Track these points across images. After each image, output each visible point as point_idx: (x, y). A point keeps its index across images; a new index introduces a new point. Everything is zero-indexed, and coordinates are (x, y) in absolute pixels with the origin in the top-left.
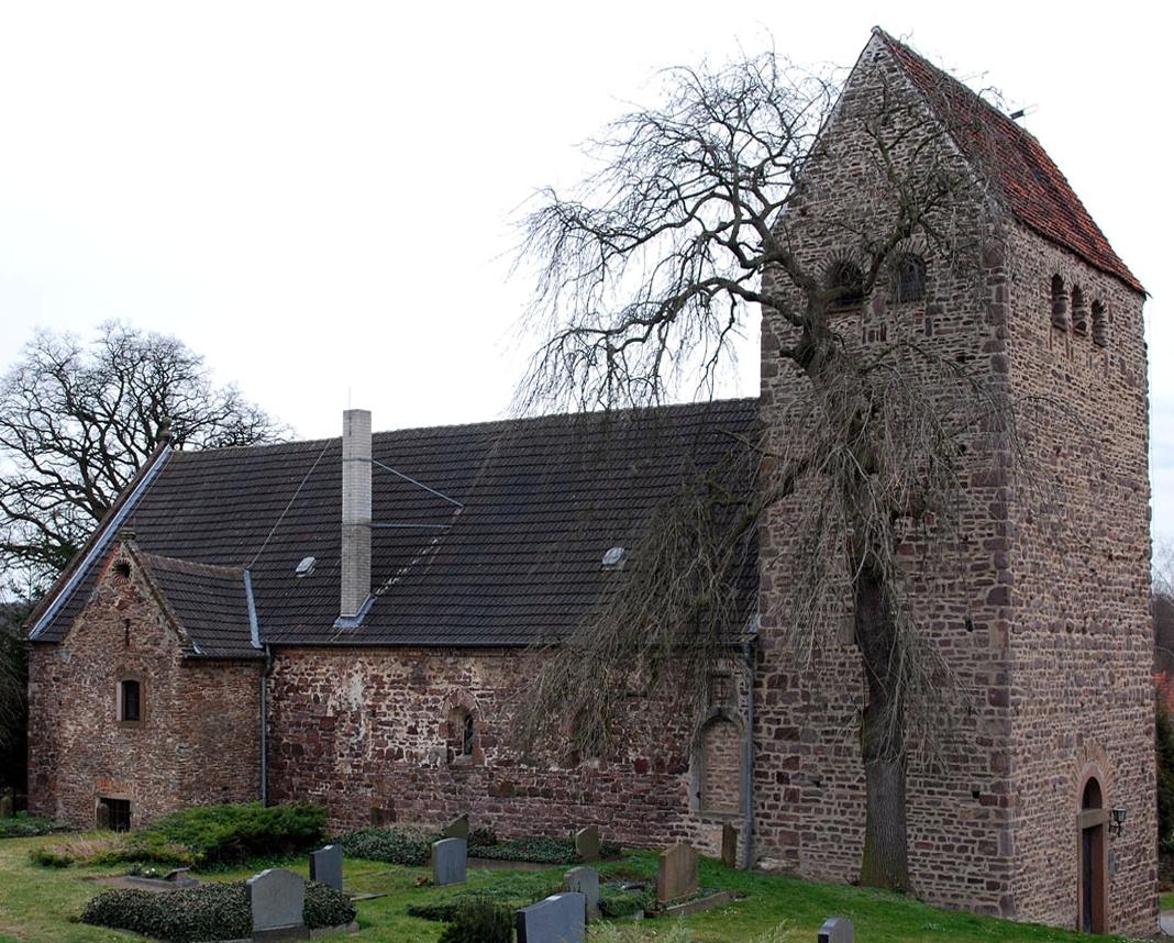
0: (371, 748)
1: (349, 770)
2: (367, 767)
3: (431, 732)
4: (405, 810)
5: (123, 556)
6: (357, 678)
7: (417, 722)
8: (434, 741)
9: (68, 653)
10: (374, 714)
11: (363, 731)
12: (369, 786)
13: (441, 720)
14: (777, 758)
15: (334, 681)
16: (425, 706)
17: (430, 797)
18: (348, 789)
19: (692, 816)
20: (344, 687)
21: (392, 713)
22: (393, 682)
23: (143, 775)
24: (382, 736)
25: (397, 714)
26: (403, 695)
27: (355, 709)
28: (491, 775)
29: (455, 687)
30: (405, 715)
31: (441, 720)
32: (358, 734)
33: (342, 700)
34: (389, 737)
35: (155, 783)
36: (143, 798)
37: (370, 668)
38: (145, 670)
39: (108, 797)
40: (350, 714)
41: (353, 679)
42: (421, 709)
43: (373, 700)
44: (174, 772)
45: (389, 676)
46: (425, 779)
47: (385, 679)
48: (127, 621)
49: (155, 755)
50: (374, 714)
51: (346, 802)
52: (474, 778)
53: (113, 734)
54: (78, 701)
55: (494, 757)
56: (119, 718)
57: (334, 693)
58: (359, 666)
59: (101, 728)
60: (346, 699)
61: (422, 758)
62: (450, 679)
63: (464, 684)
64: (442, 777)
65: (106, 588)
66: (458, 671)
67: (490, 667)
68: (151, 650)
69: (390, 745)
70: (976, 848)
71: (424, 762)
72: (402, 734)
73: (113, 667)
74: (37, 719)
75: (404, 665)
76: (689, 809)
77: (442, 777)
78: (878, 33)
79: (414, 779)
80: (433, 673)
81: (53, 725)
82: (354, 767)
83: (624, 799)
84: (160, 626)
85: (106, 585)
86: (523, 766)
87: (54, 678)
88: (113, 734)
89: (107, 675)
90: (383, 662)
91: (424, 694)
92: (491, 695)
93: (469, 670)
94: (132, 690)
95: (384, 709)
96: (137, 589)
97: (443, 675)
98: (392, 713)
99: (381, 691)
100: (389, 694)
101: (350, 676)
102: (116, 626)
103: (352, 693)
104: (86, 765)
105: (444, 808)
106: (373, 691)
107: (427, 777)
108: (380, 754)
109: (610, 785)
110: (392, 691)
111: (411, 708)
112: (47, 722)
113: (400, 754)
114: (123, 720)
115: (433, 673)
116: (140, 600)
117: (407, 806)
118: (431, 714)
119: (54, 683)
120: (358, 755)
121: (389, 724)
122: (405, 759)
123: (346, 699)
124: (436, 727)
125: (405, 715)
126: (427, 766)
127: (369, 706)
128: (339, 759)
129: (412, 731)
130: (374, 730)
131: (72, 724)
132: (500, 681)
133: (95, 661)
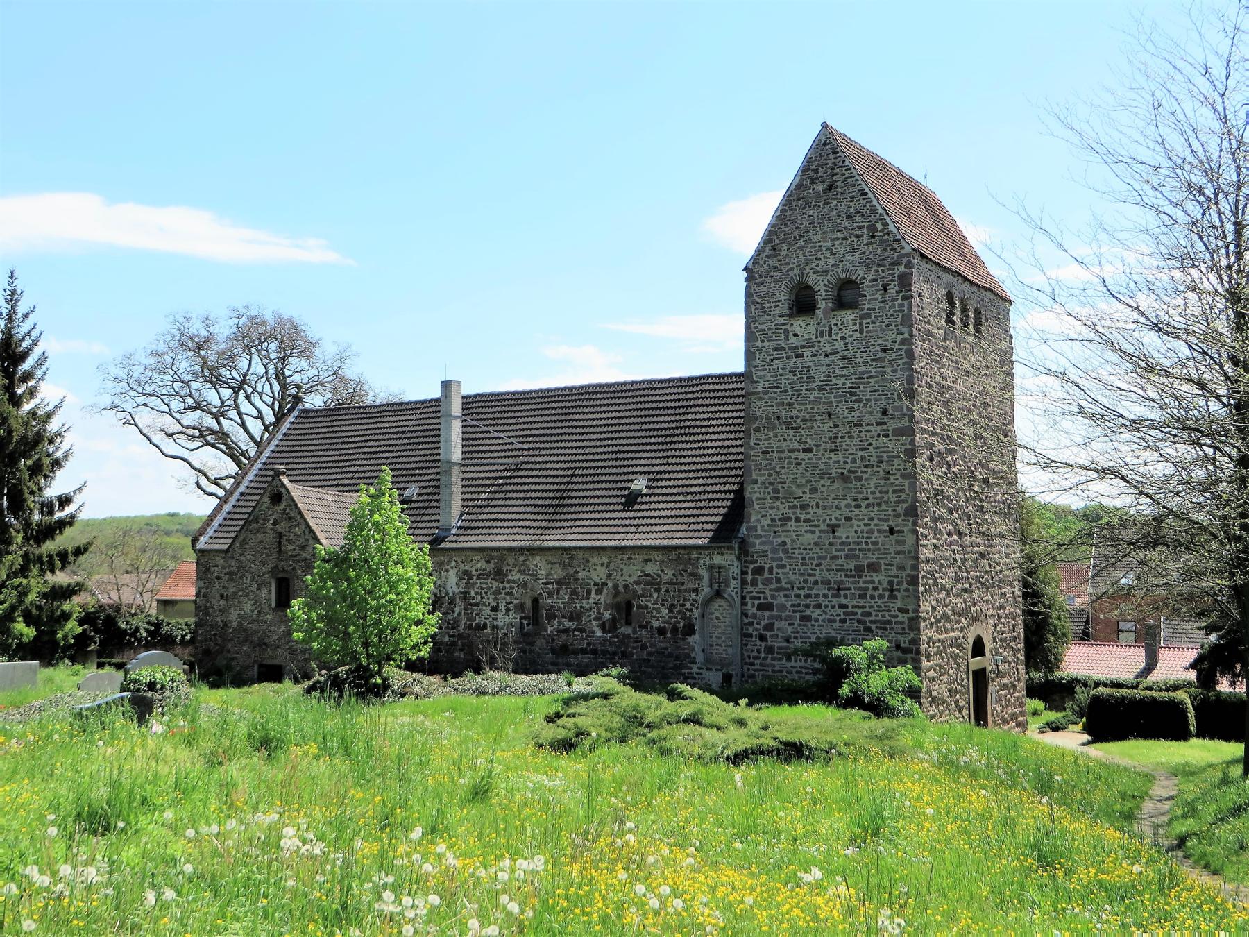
3: (508, 610)
28: (553, 640)
56: (273, 604)
96: (288, 511)
102: (270, 537)
111: (494, 593)
116: (290, 518)
129: (494, 609)
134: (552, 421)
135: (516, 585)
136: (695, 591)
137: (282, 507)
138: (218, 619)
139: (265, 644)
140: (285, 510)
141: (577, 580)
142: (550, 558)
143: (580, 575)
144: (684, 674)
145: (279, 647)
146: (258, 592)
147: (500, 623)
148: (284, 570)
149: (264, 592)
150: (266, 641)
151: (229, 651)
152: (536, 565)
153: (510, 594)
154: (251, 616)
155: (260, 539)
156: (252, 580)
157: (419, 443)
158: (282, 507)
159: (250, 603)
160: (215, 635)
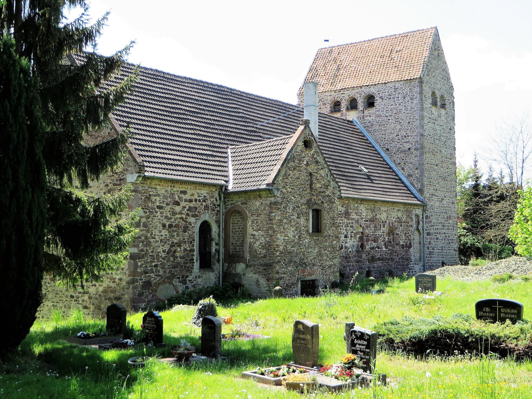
3: (351, 237)
23: (323, 263)
28: (369, 254)
35: (329, 267)
39: (306, 279)
42: (348, 227)
46: (350, 258)
48: (311, 174)
49: (329, 251)
52: (364, 256)
54: (285, 221)
56: (311, 231)
70: (54, 304)
74: (143, 238)
77: (355, 256)
79: (346, 258)
80: (351, 211)
81: (157, 242)
84: (328, 179)
86: (377, 249)
87: (157, 206)
92: (367, 221)
94: (317, 213)
96: (315, 156)
97: (354, 212)
102: (304, 176)
111: (345, 227)
112: (152, 240)
114: (313, 232)
116: (317, 162)
118: (351, 229)
119: (158, 210)
126: (350, 252)
129: (346, 237)
134: (159, 114)
135: (354, 221)
136: (411, 226)
137: (312, 152)
138: (160, 249)
139: (305, 263)
140: (313, 155)
141: (376, 219)
142: (367, 206)
143: (378, 216)
144: (409, 267)
145: (314, 265)
146: (298, 220)
147: (348, 245)
148: (316, 204)
149: (302, 221)
150: (305, 261)
151: (277, 273)
152: (361, 210)
153: (352, 227)
154: (294, 241)
155: (297, 176)
156: (293, 210)
157: (127, 112)
158: (312, 152)
159: (292, 229)
160: (156, 266)
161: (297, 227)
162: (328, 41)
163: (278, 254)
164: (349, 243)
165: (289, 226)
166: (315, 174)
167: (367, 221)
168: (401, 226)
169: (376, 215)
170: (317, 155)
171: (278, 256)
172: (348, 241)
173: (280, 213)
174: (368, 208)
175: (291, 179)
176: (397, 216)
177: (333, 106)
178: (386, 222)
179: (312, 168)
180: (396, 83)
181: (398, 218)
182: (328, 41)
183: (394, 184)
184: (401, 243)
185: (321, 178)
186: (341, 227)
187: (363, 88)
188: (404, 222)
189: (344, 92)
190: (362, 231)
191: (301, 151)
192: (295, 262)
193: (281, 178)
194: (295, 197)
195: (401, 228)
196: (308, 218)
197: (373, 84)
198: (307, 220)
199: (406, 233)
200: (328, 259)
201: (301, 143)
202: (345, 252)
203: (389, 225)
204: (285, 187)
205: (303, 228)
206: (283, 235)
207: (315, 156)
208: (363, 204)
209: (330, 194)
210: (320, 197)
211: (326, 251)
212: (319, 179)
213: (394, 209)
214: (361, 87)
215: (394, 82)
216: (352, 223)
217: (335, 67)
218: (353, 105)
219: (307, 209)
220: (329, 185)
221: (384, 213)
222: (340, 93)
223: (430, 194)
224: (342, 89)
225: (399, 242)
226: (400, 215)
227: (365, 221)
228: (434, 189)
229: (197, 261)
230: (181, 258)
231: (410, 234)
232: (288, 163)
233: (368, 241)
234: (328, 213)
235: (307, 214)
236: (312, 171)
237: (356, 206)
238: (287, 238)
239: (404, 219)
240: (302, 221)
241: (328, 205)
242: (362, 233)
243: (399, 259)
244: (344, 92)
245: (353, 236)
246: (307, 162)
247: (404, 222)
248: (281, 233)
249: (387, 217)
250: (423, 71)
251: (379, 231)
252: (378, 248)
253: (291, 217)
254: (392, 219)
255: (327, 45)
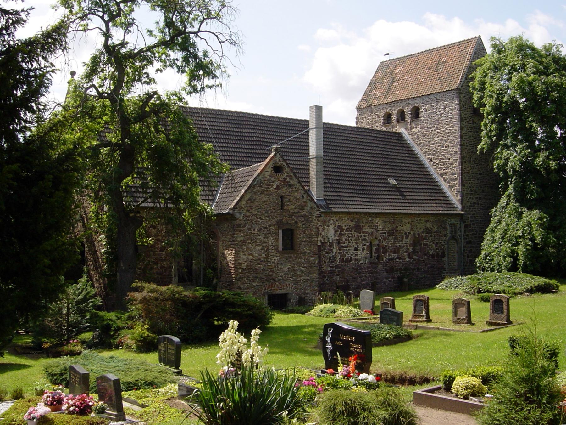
0: (338, 258)
1: (329, 269)
2: (337, 266)
3: (363, 249)
4: (354, 283)
5: (279, 161)
6: (331, 227)
7: (358, 245)
8: (365, 253)
9: (241, 213)
10: (339, 243)
11: (334, 251)
12: (337, 275)
13: (367, 244)
14: (467, 250)
15: (321, 228)
16: (361, 238)
17: (363, 276)
18: (328, 277)
19: (447, 271)
20: (326, 231)
21: (347, 242)
22: (347, 228)
24: (343, 252)
25: (349, 242)
26: (352, 234)
27: (331, 241)
28: (386, 264)
29: (372, 230)
30: (353, 243)
31: (367, 244)
32: (332, 252)
33: (325, 237)
34: (346, 253)
36: (296, 291)
37: (337, 223)
38: (296, 222)
39: (274, 293)
40: (328, 243)
41: (330, 227)
42: (359, 240)
43: (338, 237)
44: (315, 275)
45: (345, 226)
46: (361, 269)
47: (344, 227)
48: (282, 197)
50: (339, 243)
51: (328, 284)
52: (380, 267)
53: (276, 258)
55: (387, 257)
56: (281, 248)
57: (321, 234)
58: (332, 222)
59: (267, 256)
60: (327, 237)
61: (360, 261)
62: (370, 227)
63: (375, 229)
64: (368, 268)
65: (266, 177)
66: (373, 223)
67: (385, 222)
68: (299, 212)
69: (347, 255)
71: (361, 262)
72: (352, 251)
73: (273, 222)
75: (352, 221)
76: (446, 269)
77: (368, 268)
78: (479, 37)
79: (357, 270)
80: (364, 225)
82: (331, 267)
83: (428, 268)
85: (266, 175)
86: (397, 260)
88: (276, 258)
89: (270, 226)
90: (343, 220)
91: (360, 233)
92: (385, 233)
93: (377, 223)
95: (344, 240)
96: (288, 180)
98: (347, 242)
99: (342, 232)
100: (346, 234)
101: (328, 226)
102: (274, 199)
103: (330, 234)
104: (256, 277)
105: (369, 280)
106: (338, 233)
107: (362, 268)
108: (342, 261)
109: (424, 264)
110: (347, 233)
113: (351, 260)
114: (283, 249)
115: (364, 225)
116: (290, 185)
117: (354, 281)
118: (363, 242)
120: (332, 262)
121: (346, 247)
122: (353, 261)
123: (327, 237)
124: (365, 247)
125: (353, 243)
126: (362, 263)
127: (337, 240)
128: (324, 264)
129: (356, 249)
130: (340, 250)
131: (245, 255)
132: (388, 228)
133: (260, 218)
136: (445, 236)
139: (274, 279)
142: (384, 219)
147: (359, 257)
149: (271, 240)
159: (258, 248)
161: (263, 246)
162: (388, 54)
163: (240, 271)
164: (361, 255)
165: (254, 245)
166: (288, 197)
167: (385, 233)
168: (431, 236)
169: (397, 227)
170: (290, 179)
171: (240, 273)
172: (359, 253)
173: (242, 234)
174: (386, 221)
175: (257, 203)
176: (425, 227)
177: (386, 118)
178: (409, 233)
179: (284, 191)
180: (437, 95)
181: (427, 228)
182: (388, 54)
183: (429, 194)
184: (431, 253)
185: (295, 199)
186: (350, 241)
187: (410, 100)
188: (434, 232)
189: (394, 105)
190: (377, 243)
191: (270, 176)
192: (261, 278)
193: (244, 203)
194: (262, 219)
195: (430, 239)
196: (277, 237)
197: (418, 96)
198: (277, 240)
199: (437, 243)
200: (303, 274)
201: (269, 170)
202: (355, 264)
203: (415, 237)
204: (249, 211)
205: (272, 247)
206: (247, 254)
207: (288, 180)
208: (379, 217)
209: (307, 214)
210: (293, 217)
211: (301, 267)
212: (292, 201)
213: (420, 220)
214: (408, 99)
215: (436, 94)
216: (365, 236)
217: (390, 79)
218: (402, 116)
219: (276, 229)
220: (305, 206)
221: (407, 224)
222: (391, 105)
223: (471, 203)
224: (392, 102)
225: (428, 252)
226: (429, 225)
227: (381, 233)
228: (477, 198)
229: (175, 276)
230: (157, 273)
231: (443, 243)
232: (254, 188)
233: (385, 252)
234: (304, 232)
235: (277, 234)
236: (284, 194)
237: (370, 219)
238: (251, 257)
239: (434, 230)
240: (271, 240)
241: (303, 225)
242: (378, 245)
243: (428, 268)
244: (394, 105)
245: (366, 248)
246: (277, 186)
247: (434, 232)
248: (243, 252)
249: (412, 228)
250: (461, 81)
251: (401, 243)
252: (400, 258)
253: (257, 238)
254: (419, 230)
255: (387, 58)
